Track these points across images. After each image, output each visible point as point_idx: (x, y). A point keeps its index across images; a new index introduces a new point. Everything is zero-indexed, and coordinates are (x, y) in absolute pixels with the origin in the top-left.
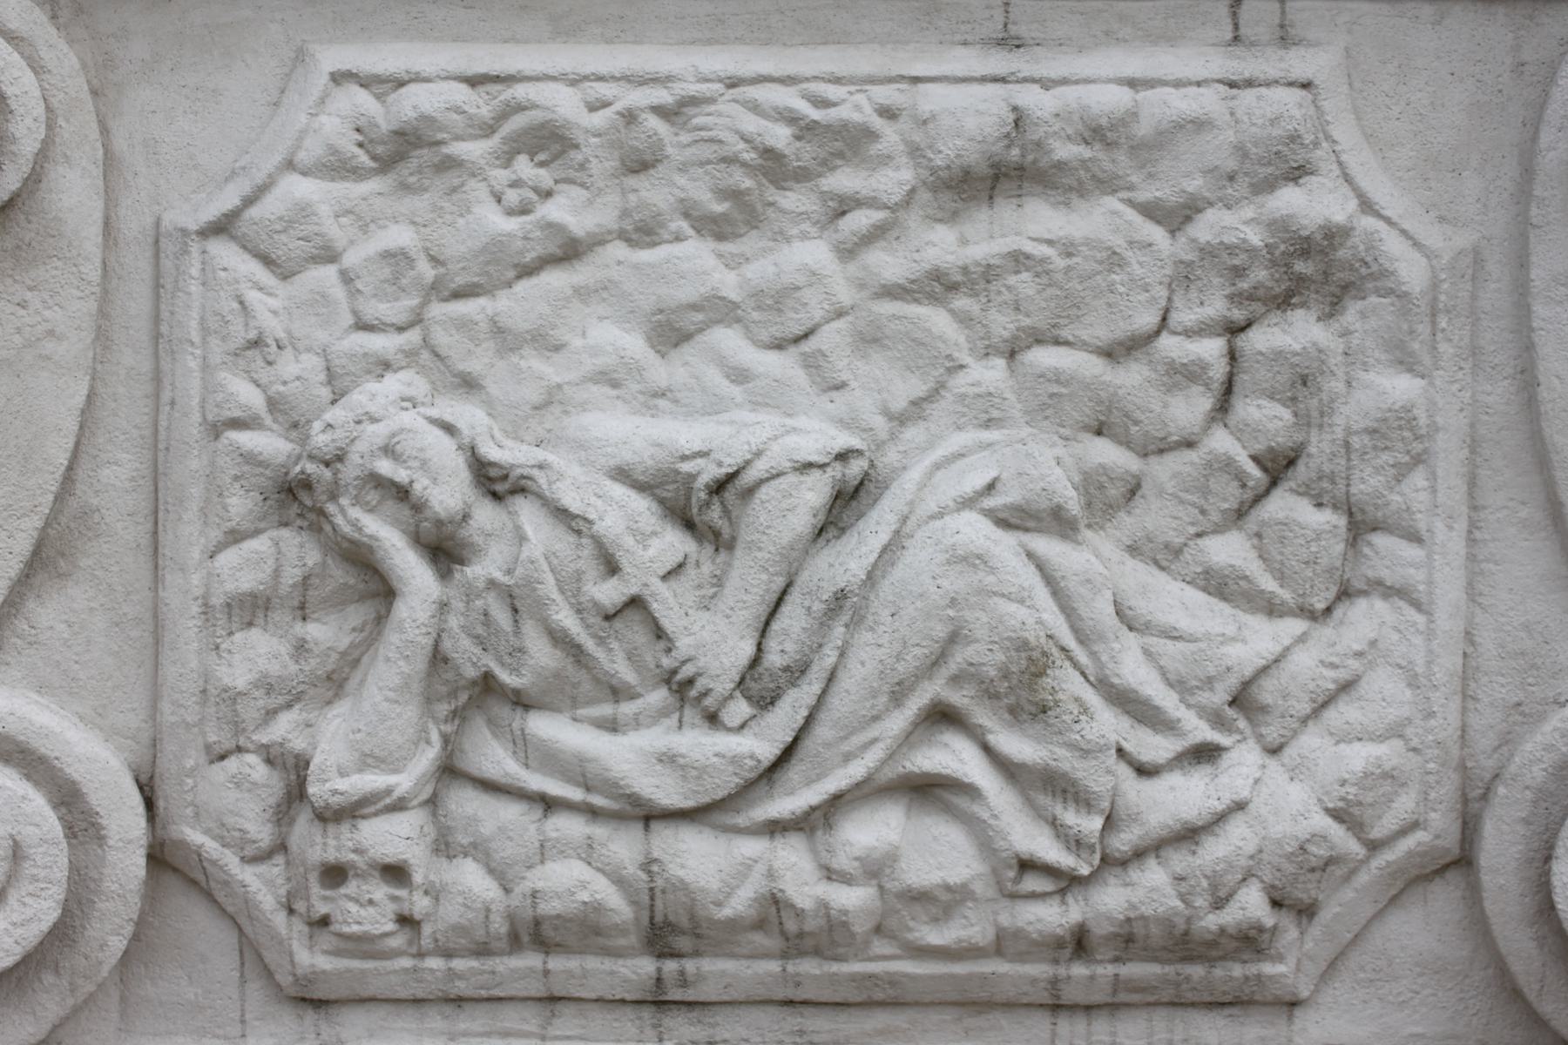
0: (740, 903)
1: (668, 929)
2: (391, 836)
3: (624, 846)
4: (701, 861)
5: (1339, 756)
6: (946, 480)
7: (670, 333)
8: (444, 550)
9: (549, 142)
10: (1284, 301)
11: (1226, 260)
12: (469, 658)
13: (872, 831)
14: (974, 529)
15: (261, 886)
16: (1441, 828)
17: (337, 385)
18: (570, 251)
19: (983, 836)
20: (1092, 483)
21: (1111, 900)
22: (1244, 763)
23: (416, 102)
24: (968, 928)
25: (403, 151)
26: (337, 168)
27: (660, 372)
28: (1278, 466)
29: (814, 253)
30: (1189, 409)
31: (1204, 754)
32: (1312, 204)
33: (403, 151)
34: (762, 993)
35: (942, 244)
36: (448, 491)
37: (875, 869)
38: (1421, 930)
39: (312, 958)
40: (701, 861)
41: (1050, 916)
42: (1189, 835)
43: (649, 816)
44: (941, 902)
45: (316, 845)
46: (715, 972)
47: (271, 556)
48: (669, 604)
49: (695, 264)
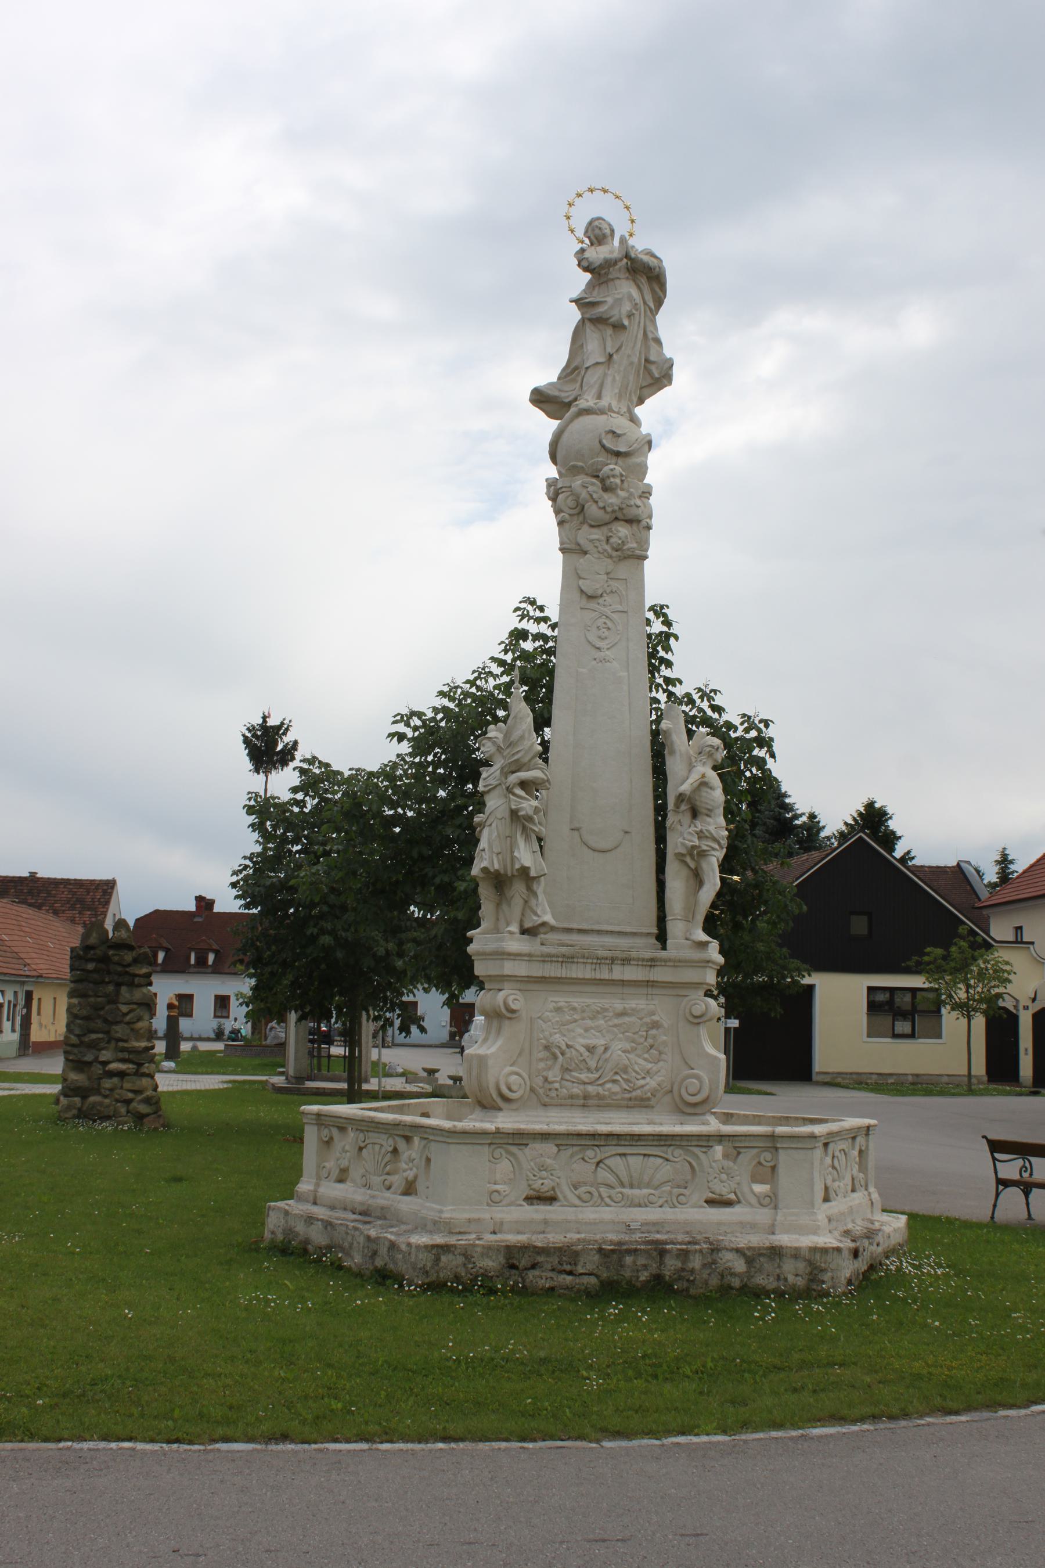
0: (594, 1093)
1: (586, 1097)
2: (557, 1085)
3: (582, 1087)
4: (590, 1089)
5: (658, 1078)
6: (617, 1046)
7: (586, 1030)
8: (563, 1054)
9: (574, 1009)
10: (652, 1028)
11: (646, 1024)
12: (565, 1066)
13: (608, 1085)
14: (620, 1052)
15: (541, 1091)
16: (669, 1088)
17: (551, 1035)
18: (576, 1021)
19: (620, 1086)
20: (632, 1047)
21: (634, 1094)
22: (648, 1079)
23: (560, 1004)
24: (619, 1097)
25: (558, 1010)
26: (551, 1011)
27: (586, 1035)
28: (652, 1047)
29: (602, 1022)
30: (642, 1040)
31: (644, 1078)
32: (656, 1018)
33: (558, 1010)
34: (995, 910)
35: (616, 1021)
36: (564, 1047)
37: (609, 1090)
38: (667, 1099)
39: (547, 1100)
40: (590, 1089)
41: (627, 1096)
42: (642, 1086)
43: (585, 1083)
44: (615, 1094)
45: (548, 1086)
46: (590, 1102)
47: (543, 1054)
48: (588, 1060)
49: (589, 1023)
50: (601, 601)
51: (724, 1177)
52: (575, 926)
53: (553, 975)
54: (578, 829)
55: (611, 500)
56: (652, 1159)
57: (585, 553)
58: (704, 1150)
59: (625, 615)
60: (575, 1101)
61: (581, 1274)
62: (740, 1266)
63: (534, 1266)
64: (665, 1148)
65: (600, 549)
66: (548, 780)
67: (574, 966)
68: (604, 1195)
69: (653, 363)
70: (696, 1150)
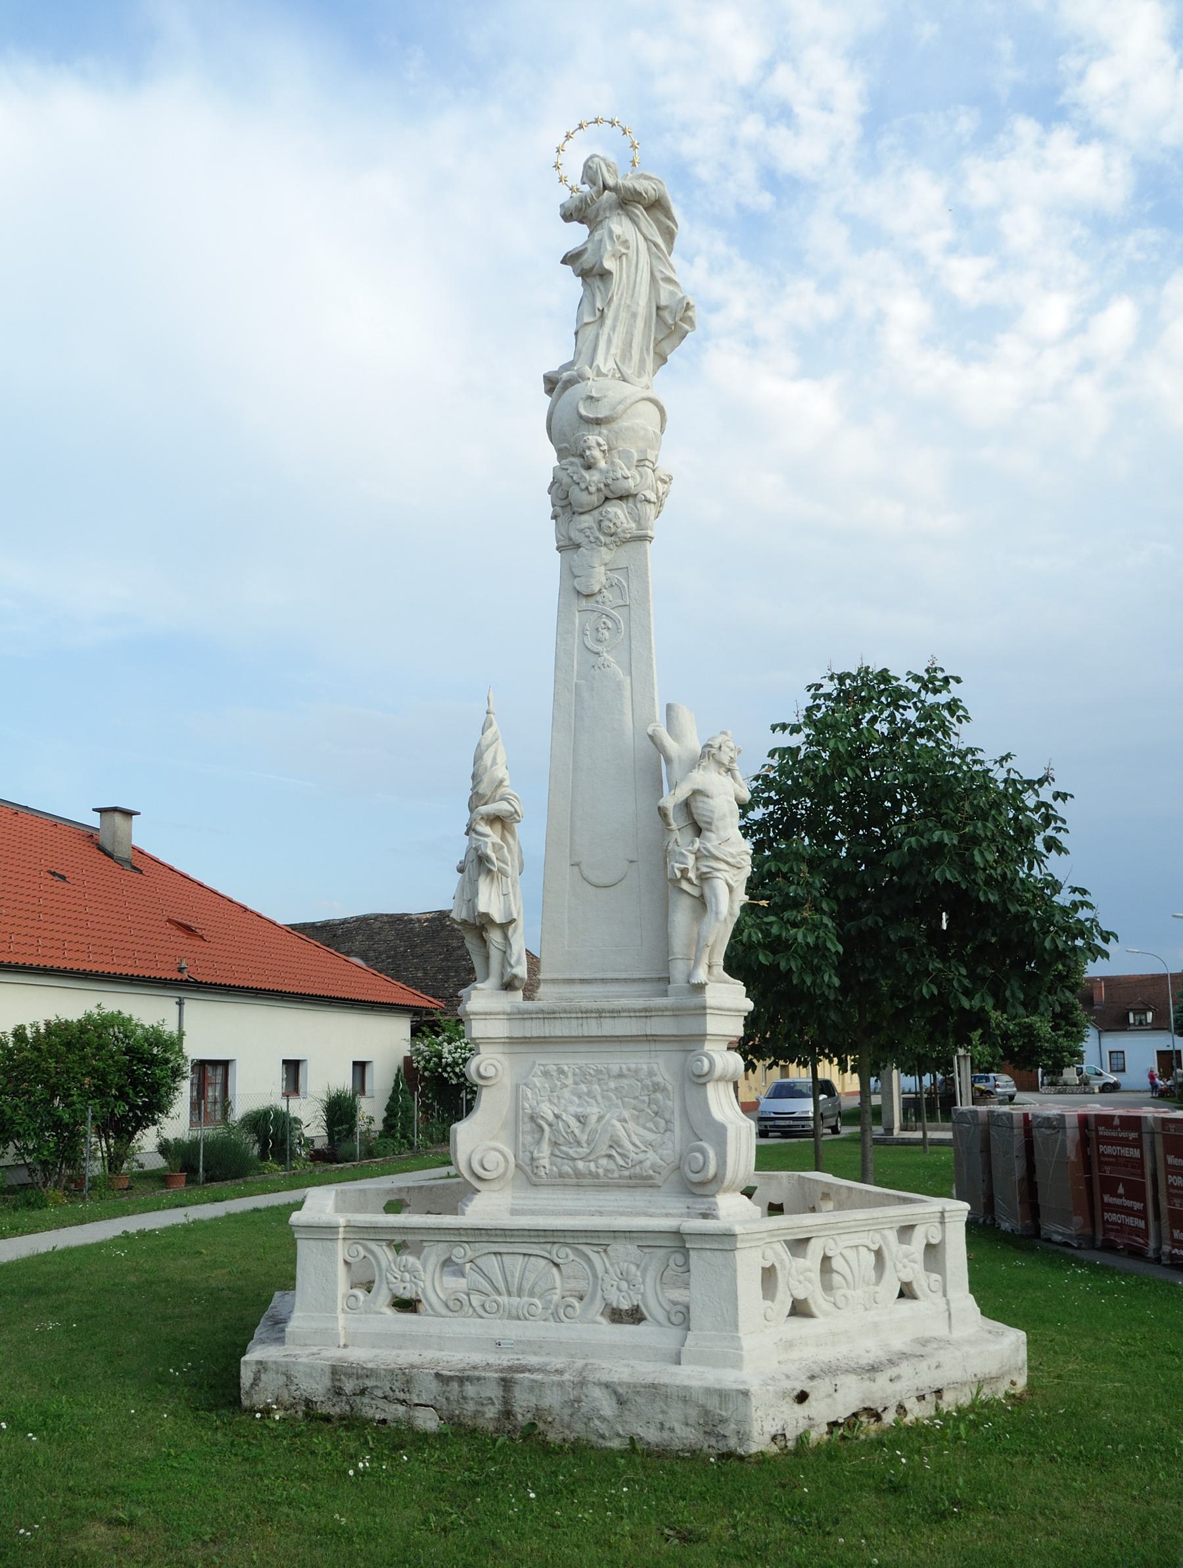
1: (578, 1174)
4: (580, 1165)
12: (553, 1139)
41: (626, 1173)
47: (528, 1126)
50: (599, 598)
51: (624, 1285)
52: (577, 976)
53: (535, 1035)
54: (578, 864)
55: (593, 477)
56: (532, 1258)
57: (578, 546)
58: (595, 1249)
59: (626, 609)
60: (567, 1181)
61: (417, 1405)
62: (608, 1407)
63: (363, 1392)
64: (548, 1246)
65: (592, 539)
66: (516, 812)
67: (558, 1022)
68: (475, 1303)
69: (666, 307)
70: (587, 1250)
